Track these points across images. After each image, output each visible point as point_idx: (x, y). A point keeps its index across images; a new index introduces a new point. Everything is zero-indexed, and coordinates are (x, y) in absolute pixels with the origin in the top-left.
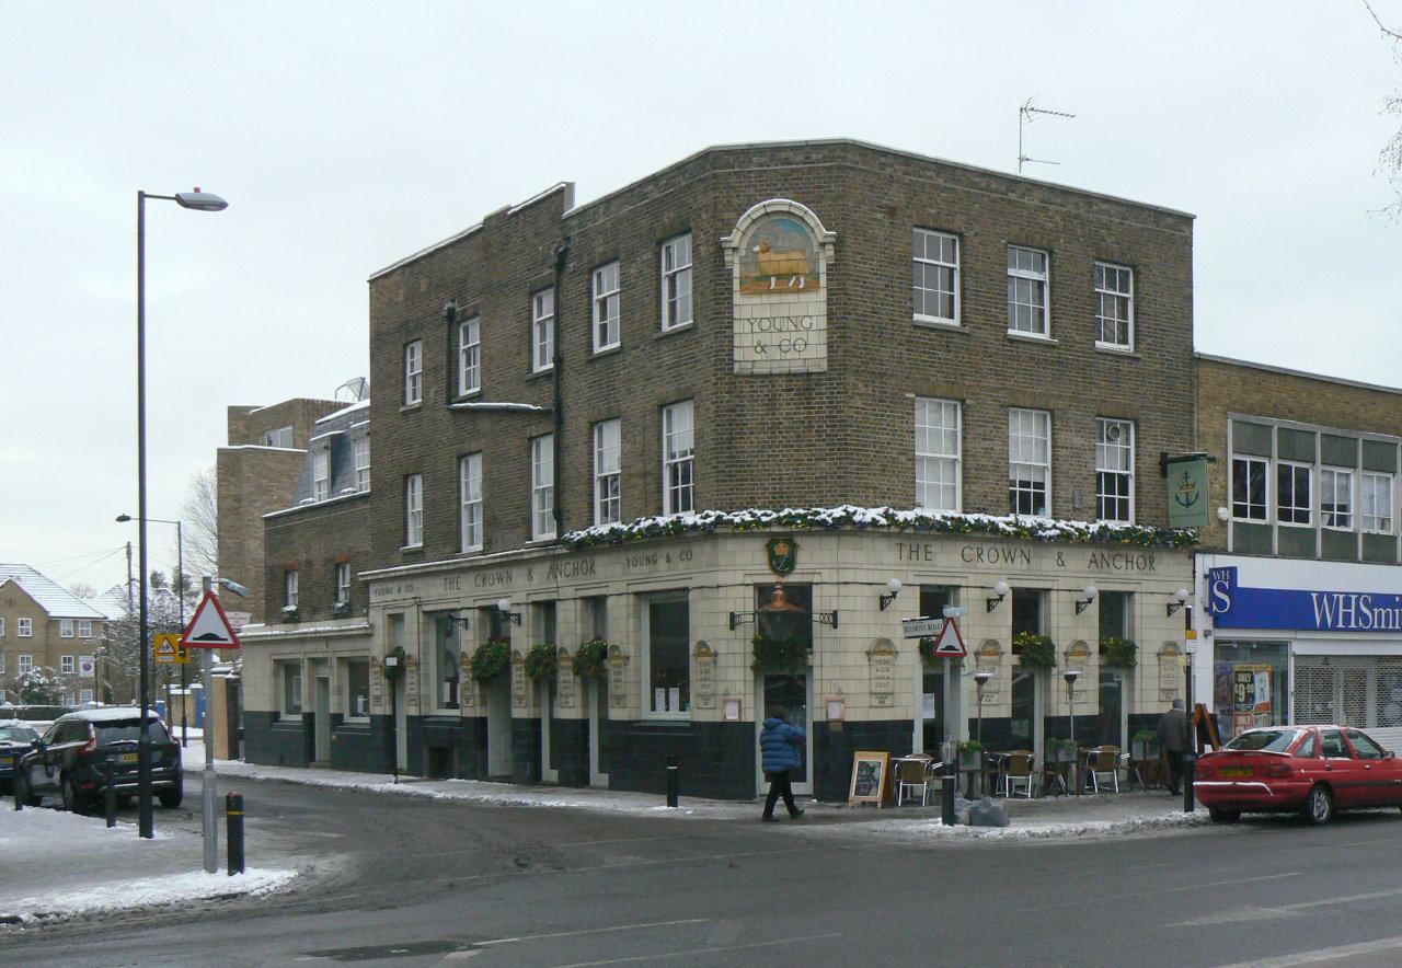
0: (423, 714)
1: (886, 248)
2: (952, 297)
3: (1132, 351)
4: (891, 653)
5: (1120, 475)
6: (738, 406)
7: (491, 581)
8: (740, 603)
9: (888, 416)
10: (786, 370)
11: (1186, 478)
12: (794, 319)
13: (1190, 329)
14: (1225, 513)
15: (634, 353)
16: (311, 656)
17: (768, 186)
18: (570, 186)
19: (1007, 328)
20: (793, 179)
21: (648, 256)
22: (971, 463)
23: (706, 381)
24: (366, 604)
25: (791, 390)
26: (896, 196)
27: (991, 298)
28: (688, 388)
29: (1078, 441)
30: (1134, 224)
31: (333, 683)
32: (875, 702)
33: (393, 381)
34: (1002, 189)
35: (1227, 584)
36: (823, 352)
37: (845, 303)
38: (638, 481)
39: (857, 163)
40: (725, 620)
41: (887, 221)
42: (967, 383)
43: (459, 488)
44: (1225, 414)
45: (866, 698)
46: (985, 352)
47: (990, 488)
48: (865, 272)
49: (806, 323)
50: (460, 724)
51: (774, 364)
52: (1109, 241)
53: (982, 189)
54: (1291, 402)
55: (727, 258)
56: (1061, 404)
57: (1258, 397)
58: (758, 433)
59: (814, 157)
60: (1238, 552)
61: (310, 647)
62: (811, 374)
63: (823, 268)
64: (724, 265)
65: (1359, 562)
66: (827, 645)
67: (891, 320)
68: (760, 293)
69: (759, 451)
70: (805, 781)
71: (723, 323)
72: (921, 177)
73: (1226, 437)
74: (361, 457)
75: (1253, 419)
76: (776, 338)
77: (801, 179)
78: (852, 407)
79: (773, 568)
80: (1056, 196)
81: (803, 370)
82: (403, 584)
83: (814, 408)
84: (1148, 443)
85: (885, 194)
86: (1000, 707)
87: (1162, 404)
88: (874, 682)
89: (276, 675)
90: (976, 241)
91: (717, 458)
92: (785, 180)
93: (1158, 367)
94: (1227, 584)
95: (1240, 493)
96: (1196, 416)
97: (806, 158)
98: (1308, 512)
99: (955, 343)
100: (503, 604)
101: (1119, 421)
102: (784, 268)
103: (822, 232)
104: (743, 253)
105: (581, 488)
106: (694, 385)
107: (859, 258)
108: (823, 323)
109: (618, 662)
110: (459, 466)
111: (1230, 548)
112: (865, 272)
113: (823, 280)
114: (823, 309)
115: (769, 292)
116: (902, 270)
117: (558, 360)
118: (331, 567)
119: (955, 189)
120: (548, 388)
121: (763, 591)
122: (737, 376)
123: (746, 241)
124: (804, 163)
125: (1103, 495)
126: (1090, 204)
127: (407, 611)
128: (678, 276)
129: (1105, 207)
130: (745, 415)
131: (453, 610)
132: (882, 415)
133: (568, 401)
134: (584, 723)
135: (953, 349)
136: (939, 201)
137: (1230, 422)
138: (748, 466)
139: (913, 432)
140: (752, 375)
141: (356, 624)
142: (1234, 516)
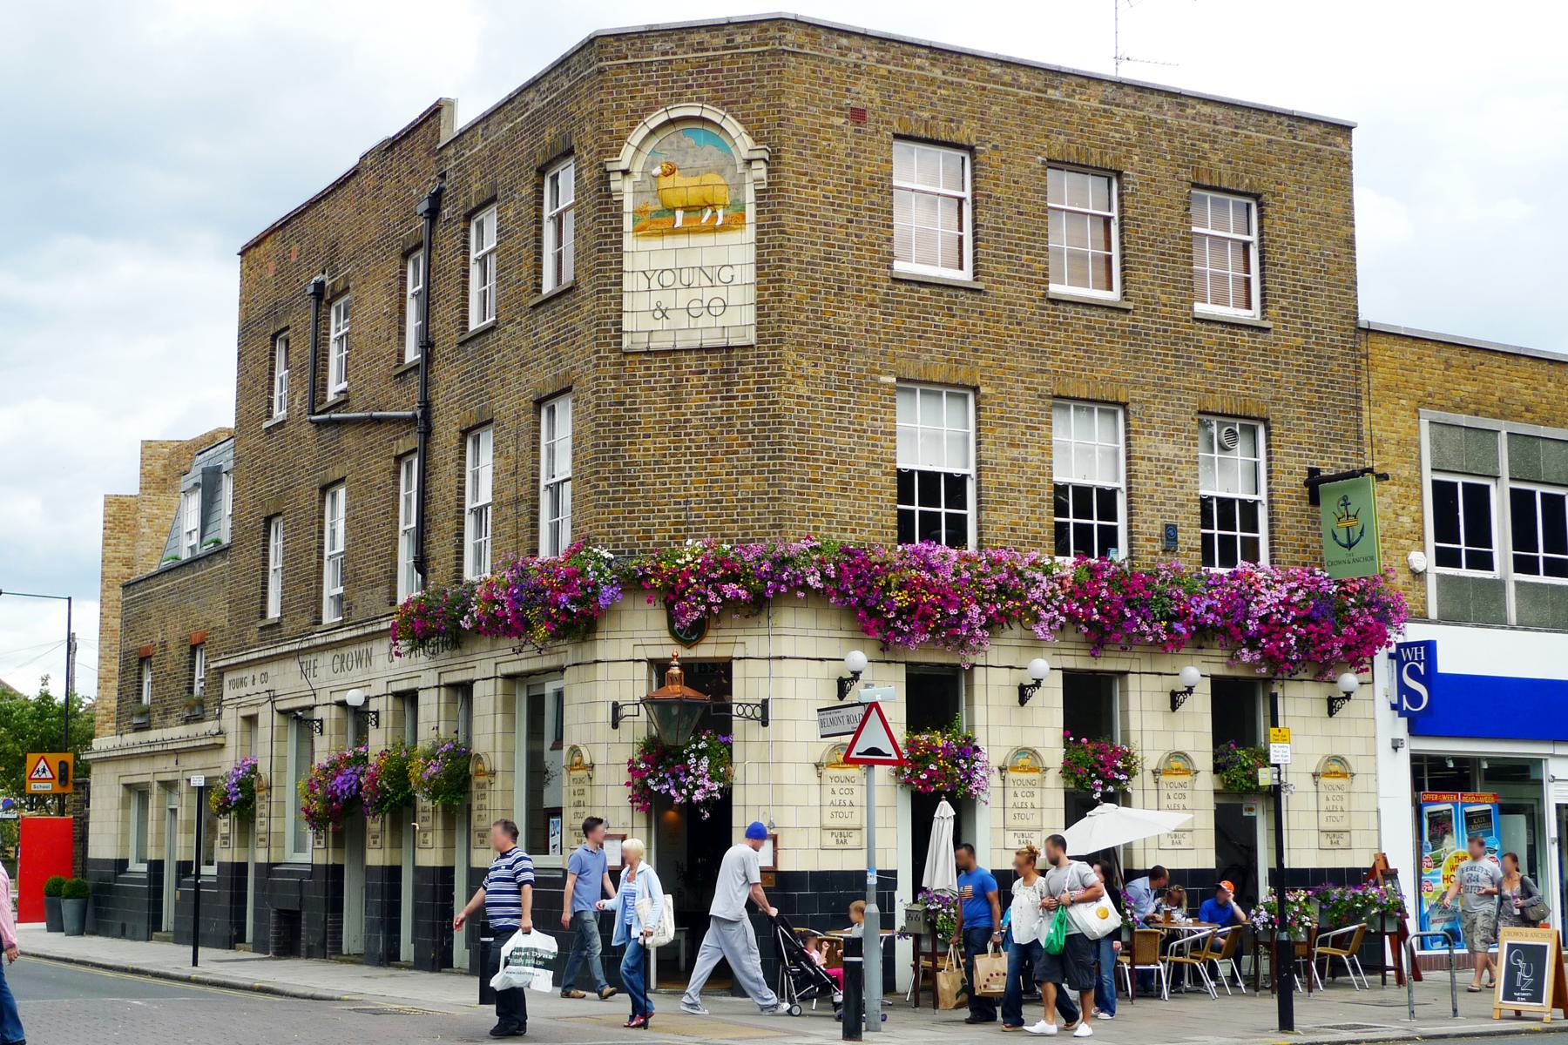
0: (272, 861)
1: (848, 167)
3: (1258, 317)
4: (1186, 772)
5: (1243, 502)
6: (627, 396)
8: (627, 687)
9: (852, 409)
10: (696, 345)
11: (1346, 504)
12: (708, 272)
13: (1353, 285)
14: (1424, 559)
17: (673, 82)
18: (451, 104)
19: (1047, 282)
20: (710, 71)
21: (527, 190)
22: (989, 480)
23: (586, 363)
24: (219, 703)
25: (705, 372)
26: (866, 93)
27: (1020, 239)
28: (567, 374)
29: (1167, 449)
30: (1254, 134)
31: (182, 815)
33: (259, 388)
34: (1038, 84)
35: (1421, 668)
36: (750, 315)
37: (781, 246)
38: (510, 512)
39: (801, 46)
40: (605, 714)
41: (850, 129)
42: (981, 362)
43: (321, 532)
44: (1417, 411)
45: (815, 838)
46: (1010, 317)
48: (815, 202)
49: (726, 275)
50: (311, 875)
51: (680, 336)
52: (1214, 159)
53: (1004, 84)
54: (1528, 396)
55: (613, 186)
56: (1137, 394)
57: (1470, 387)
58: (657, 436)
59: (739, 39)
60: (1445, 619)
62: (733, 348)
63: (750, 196)
64: (610, 196)
66: (753, 752)
67: (856, 270)
68: (662, 234)
69: (656, 463)
71: (609, 278)
72: (905, 66)
73: (1418, 446)
75: (1464, 419)
76: (683, 298)
77: (721, 71)
78: (791, 396)
79: (674, 634)
80: (1126, 95)
81: (721, 343)
82: (257, 672)
83: (734, 398)
84: (1288, 455)
85: (848, 90)
87: (1306, 395)
88: (827, 811)
89: (125, 805)
90: (996, 156)
91: (597, 472)
92: (698, 73)
93: (1300, 340)
94: (1421, 668)
95: (1445, 529)
96: (1366, 414)
97: (728, 41)
99: (962, 303)
101: (1238, 422)
102: (694, 197)
103: (744, 144)
104: (638, 177)
105: (450, 525)
106: (574, 368)
107: (804, 180)
108: (750, 274)
110: (323, 501)
111: (1433, 613)
112: (815, 202)
113: (750, 212)
114: (750, 254)
115: (674, 232)
116: (875, 198)
118: (187, 649)
119: (960, 84)
120: (415, 381)
121: (659, 667)
122: (626, 354)
123: (642, 158)
124: (725, 48)
125: (1216, 532)
126: (1182, 106)
127: (261, 709)
129: (1207, 109)
130: (637, 410)
131: (302, 709)
132: (841, 408)
133: (438, 403)
136: (935, 100)
138: (642, 484)
139: (893, 434)
140: (648, 352)
141: (210, 726)
142: (1438, 565)
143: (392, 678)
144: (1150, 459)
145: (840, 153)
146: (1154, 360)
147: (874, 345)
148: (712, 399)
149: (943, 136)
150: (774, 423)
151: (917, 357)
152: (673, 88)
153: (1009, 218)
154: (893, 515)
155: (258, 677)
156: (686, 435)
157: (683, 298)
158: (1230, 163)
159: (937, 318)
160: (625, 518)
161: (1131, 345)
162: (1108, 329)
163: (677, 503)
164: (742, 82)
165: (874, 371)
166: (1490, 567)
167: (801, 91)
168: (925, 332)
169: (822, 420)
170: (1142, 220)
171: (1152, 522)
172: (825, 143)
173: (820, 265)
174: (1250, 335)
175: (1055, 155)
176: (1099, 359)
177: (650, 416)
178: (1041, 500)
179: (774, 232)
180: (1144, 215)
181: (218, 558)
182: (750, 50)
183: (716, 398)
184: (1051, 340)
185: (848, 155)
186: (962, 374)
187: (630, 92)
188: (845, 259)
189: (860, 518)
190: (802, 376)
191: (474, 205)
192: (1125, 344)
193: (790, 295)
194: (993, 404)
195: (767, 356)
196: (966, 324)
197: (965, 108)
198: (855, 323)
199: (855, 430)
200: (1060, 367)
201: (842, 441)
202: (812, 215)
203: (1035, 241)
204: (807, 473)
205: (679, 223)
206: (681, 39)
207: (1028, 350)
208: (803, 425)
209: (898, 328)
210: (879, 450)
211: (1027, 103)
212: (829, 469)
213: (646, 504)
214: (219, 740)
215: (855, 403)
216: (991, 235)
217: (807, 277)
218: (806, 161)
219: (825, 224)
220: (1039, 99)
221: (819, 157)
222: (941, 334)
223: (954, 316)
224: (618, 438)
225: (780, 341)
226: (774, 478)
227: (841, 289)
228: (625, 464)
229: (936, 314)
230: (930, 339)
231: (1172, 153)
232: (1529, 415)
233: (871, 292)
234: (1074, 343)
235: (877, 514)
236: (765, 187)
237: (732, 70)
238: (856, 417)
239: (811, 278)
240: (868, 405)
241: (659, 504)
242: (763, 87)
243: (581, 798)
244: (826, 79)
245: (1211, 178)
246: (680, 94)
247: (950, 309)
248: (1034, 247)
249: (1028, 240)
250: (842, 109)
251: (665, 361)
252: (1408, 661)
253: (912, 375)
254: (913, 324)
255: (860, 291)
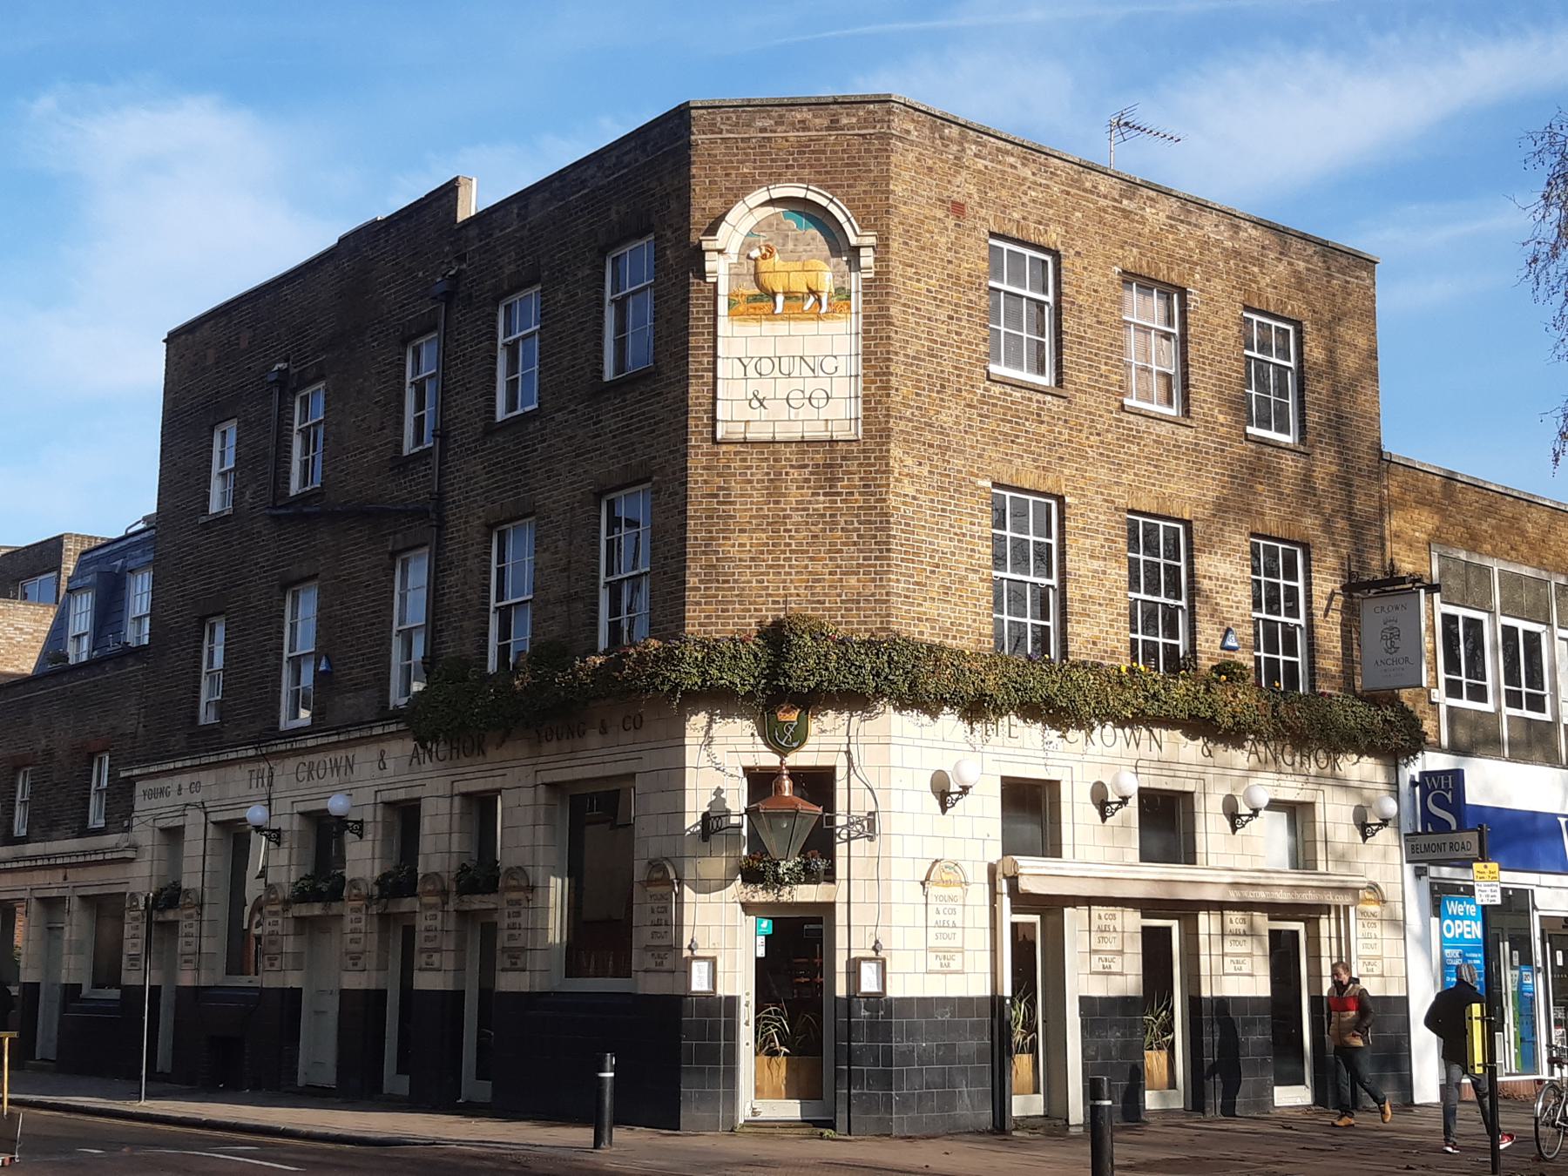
2: (1041, 345)
6: (720, 488)
7: (321, 773)
10: (798, 436)
15: (559, 416)
16: (38, 894)
17: (772, 160)
20: (813, 152)
25: (806, 466)
27: (1099, 348)
32: (935, 964)
35: (1449, 796)
42: (1066, 471)
47: (1101, 631)
48: (920, 295)
53: (1085, 190)
58: (754, 531)
61: (40, 878)
65: (1454, 832)
67: (956, 368)
70: (1082, 999)
74: (140, 596)
76: (783, 387)
77: (824, 152)
81: (825, 436)
86: (1127, 979)
90: (1078, 261)
94: (1449, 796)
98: (1544, 696)
100: (337, 804)
108: (856, 365)
109: (515, 895)
117: (442, 435)
128: (631, 302)
130: (731, 503)
134: (458, 996)
135: (1046, 419)
137: (1435, 555)
140: (745, 442)
143: (381, 788)
144: (1210, 578)
145: (942, 249)
146: (1213, 479)
147: (972, 447)
148: (813, 494)
149: (1033, 238)
150: (881, 522)
151: (1010, 462)
152: (772, 167)
153: (1090, 326)
154: (989, 623)
155: (185, 786)
156: (785, 531)
157: (783, 387)
158: (1275, 288)
159: (1027, 423)
160: (718, 617)
161: (1194, 462)
162: (1174, 446)
163: (774, 602)
164: (848, 165)
165: (972, 474)
166: (1484, 699)
167: (907, 178)
168: (1017, 437)
169: (926, 521)
170: (1203, 339)
171: (1213, 642)
172: (928, 235)
173: (924, 360)
174: (1293, 460)
175: (1129, 267)
176: (1167, 475)
177: (745, 510)
178: (1119, 614)
179: (881, 323)
180: (1205, 333)
181: (130, 661)
182: (857, 132)
183: (818, 494)
184: (1125, 453)
185: (949, 249)
186: (1049, 483)
187: (725, 168)
188: (946, 356)
189: (960, 624)
190: (908, 475)
191: (506, 288)
192: (1188, 461)
193: (897, 390)
194: (1076, 515)
195: (874, 451)
196: (1052, 431)
197: (1051, 212)
198: (955, 423)
199: (955, 534)
200: (1134, 481)
201: (944, 544)
202: (917, 309)
203: (1112, 352)
204: (912, 576)
205: (779, 309)
206: (781, 116)
207: (1107, 462)
208: (909, 525)
209: (993, 431)
210: (977, 556)
211: (1105, 211)
212: (933, 572)
213: (741, 603)
214: (130, 854)
215: (956, 505)
216: (1074, 343)
217: (913, 372)
218: (911, 251)
219: (929, 319)
220: (1115, 208)
221: (923, 248)
222: (1031, 440)
223: (1042, 422)
224: (711, 532)
225: (888, 437)
226: (881, 580)
227: (943, 386)
228: (718, 559)
229: (1027, 420)
230: (1022, 444)
231: (1228, 273)
232: (1513, 553)
233: (969, 392)
234: (1146, 458)
235: (975, 621)
236: (872, 275)
237: (836, 152)
238: (956, 520)
239: (916, 373)
240: (966, 508)
241: (755, 603)
242: (871, 171)
243: (517, 920)
244: (930, 169)
245: (1260, 302)
246: (780, 175)
247: (1039, 415)
248: (1111, 358)
249: (1106, 350)
250: (944, 202)
251: (763, 453)
252: (1433, 789)
253: (1006, 481)
254: (1006, 428)
255: (960, 390)
